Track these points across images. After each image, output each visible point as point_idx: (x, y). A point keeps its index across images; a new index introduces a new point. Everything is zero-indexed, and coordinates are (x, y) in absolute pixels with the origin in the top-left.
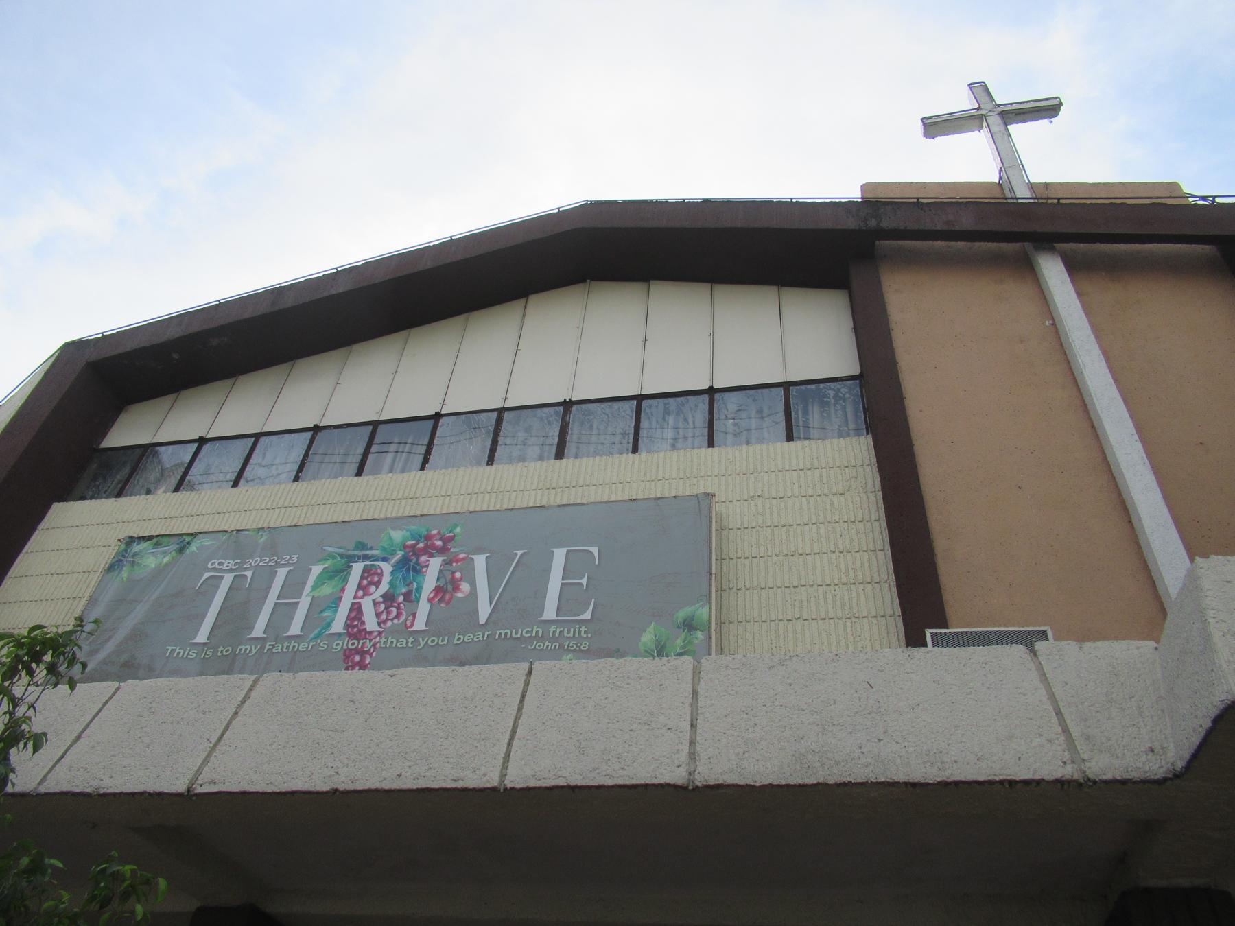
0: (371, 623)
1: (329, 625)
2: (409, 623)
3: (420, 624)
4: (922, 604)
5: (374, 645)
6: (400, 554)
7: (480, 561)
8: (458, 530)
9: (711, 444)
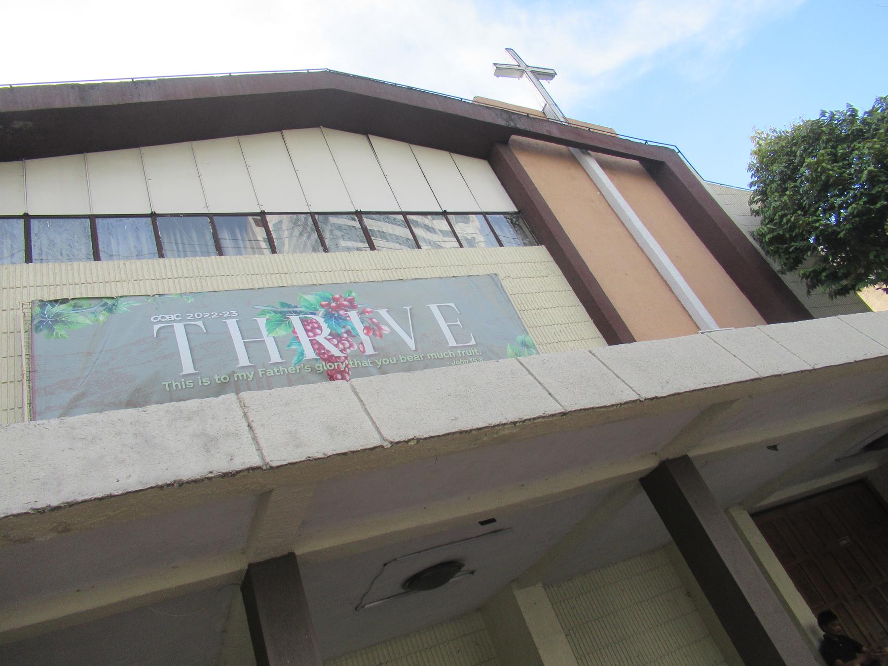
0: (335, 352)
1: (302, 354)
2: (361, 349)
3: (370, 351)
4: (613, 330)
5: (347, 366)
6: (322, 311)
7: (383, 312)
8: (354, 294)
9: (29, 259)
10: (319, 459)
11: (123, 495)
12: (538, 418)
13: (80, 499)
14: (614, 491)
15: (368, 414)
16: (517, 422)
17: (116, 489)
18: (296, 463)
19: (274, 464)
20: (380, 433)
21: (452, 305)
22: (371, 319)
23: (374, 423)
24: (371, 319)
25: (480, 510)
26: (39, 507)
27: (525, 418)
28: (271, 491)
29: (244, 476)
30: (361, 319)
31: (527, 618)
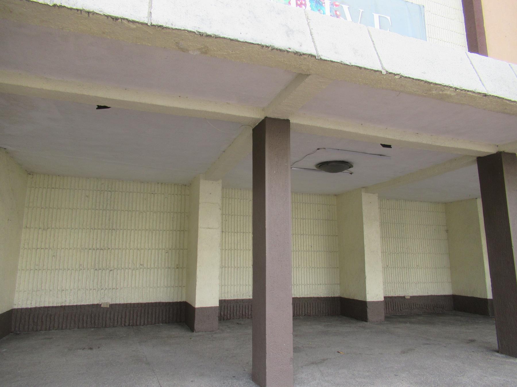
10: (347, 65)
11: (243, 42)
12: (471, 91)
13: (222, 36)
14: (455, 159)
15: (376, 50)
16: (457, 89)
17: (241, 38)
18: (334, 62)
19: (323, 58)
20: (381, 63)
21: (389, 18)
22: (336, 11)
23: (379, 57)
24: (336, 11)
25: (390, 137)
26: (201, 31)
27: (464, 88)
28: (308, 75)
29: (305, 58)
30: (330, 8)
31: (364, 207)
